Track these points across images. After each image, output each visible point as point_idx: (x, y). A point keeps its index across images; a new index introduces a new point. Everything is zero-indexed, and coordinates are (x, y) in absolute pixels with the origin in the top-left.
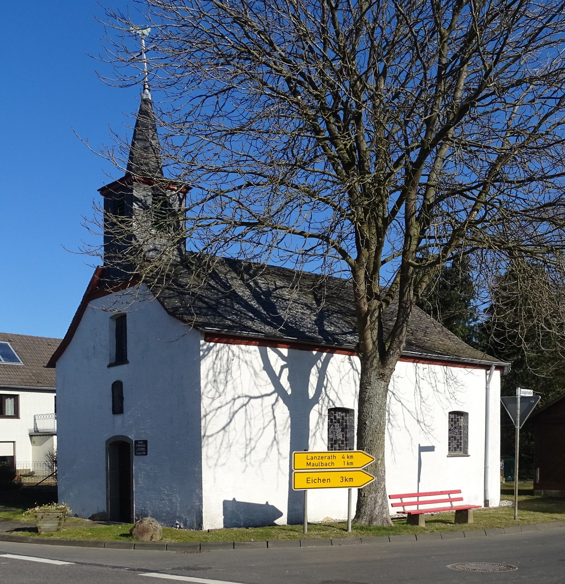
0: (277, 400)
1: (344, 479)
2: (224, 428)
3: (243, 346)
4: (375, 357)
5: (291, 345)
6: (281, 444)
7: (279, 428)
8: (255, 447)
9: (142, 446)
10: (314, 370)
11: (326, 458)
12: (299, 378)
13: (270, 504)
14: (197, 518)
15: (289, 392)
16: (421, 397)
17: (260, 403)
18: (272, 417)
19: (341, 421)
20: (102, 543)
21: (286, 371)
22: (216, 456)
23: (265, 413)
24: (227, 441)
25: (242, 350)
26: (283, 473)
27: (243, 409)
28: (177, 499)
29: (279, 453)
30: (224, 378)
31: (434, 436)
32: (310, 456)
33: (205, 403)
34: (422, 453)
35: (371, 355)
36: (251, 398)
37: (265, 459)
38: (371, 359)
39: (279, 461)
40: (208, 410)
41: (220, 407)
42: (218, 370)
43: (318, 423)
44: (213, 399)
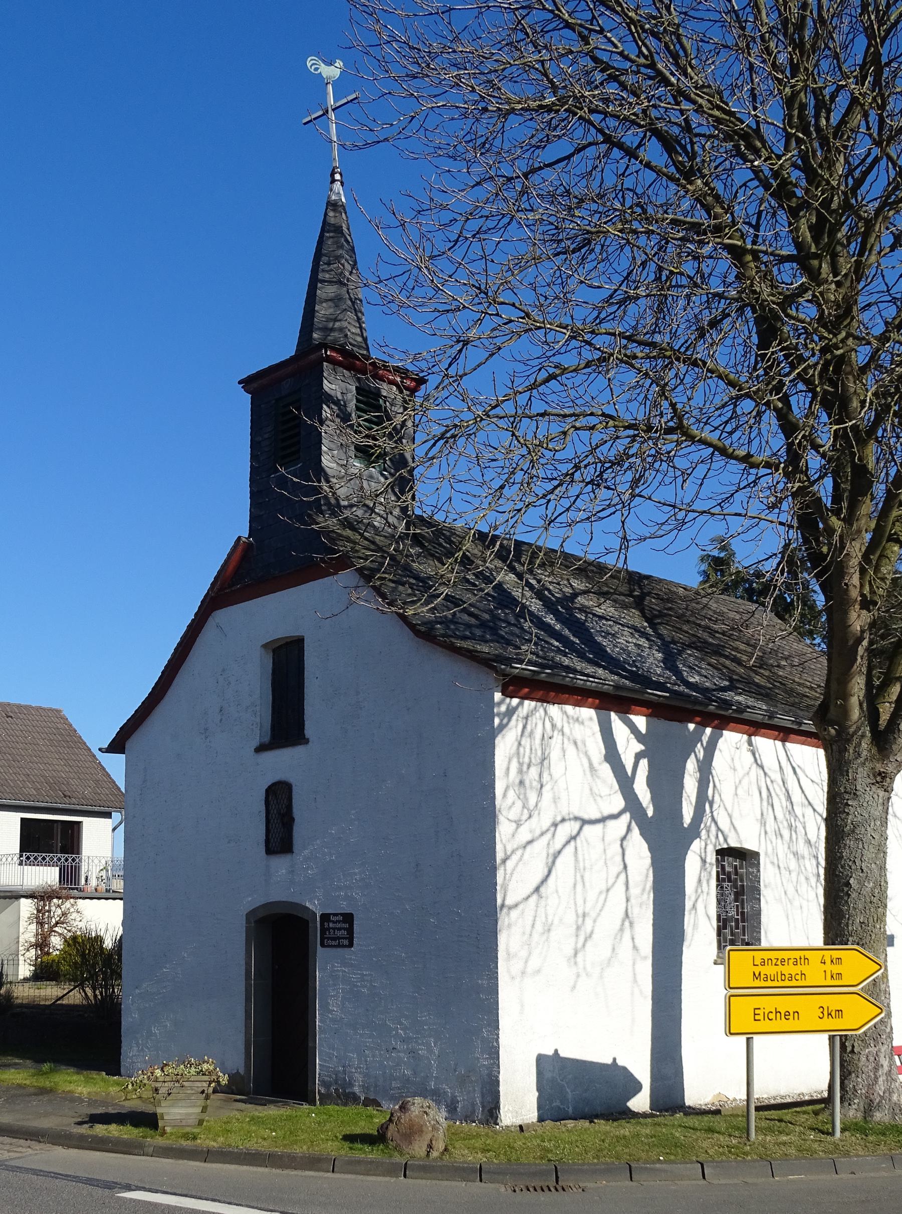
0: (629, 829)
1: (826, 1013)
2: (537, 889)
3: (569, 708)
4: (863, 736)
5: (655, 710)
6: (637, 927)
7: (634, 891)
8: (592, 932)
9: (338, 925)
10: (691, 765)
11: (791, 962)
12: (666, 783)
13: (620, 1062)
14: (483, 1096)
15: (650, 813)
17: (601, 835)
18: (622, 866)
19: (733, 877)
20: (327, 1160)
21: (644, 764)
22: (524, 953)
23: (608, 857)
24: (544, 919)
25: (568, 717)
26: (641, 992)
27: (570, 848)
28: (431, 1051)
29: (635, 947)
30: (537, 778)
32: (759, 955)
33: (504, 831)
35: (855, 733)
36: (585, 822)
37: (610, 960)
38: (855, 741)
39: (634, 964)
40: (509, 849)
41: (530, 842)
42: (526, 760)
43: (700, 881)
44: (518, 824)
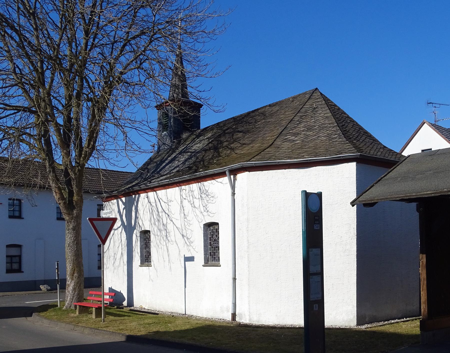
5: (124, 195)
6: (124, 257)
10: (133, 208)
16: (184, 214)
31: (194, 248)
34: (186, 262)
